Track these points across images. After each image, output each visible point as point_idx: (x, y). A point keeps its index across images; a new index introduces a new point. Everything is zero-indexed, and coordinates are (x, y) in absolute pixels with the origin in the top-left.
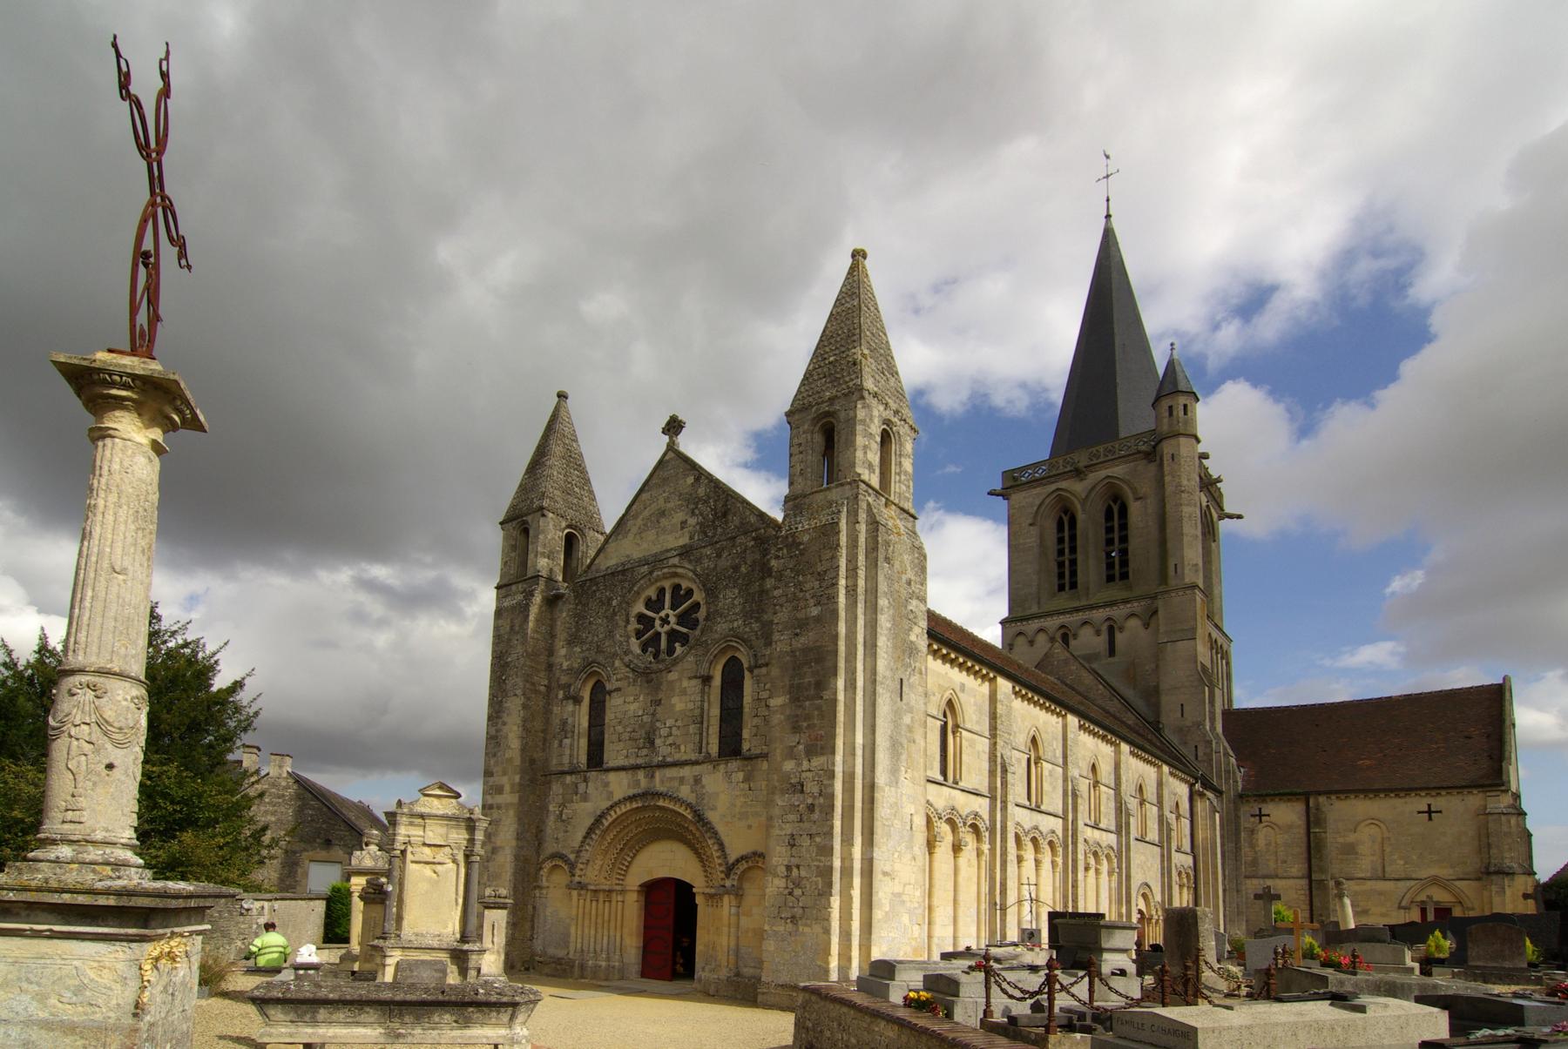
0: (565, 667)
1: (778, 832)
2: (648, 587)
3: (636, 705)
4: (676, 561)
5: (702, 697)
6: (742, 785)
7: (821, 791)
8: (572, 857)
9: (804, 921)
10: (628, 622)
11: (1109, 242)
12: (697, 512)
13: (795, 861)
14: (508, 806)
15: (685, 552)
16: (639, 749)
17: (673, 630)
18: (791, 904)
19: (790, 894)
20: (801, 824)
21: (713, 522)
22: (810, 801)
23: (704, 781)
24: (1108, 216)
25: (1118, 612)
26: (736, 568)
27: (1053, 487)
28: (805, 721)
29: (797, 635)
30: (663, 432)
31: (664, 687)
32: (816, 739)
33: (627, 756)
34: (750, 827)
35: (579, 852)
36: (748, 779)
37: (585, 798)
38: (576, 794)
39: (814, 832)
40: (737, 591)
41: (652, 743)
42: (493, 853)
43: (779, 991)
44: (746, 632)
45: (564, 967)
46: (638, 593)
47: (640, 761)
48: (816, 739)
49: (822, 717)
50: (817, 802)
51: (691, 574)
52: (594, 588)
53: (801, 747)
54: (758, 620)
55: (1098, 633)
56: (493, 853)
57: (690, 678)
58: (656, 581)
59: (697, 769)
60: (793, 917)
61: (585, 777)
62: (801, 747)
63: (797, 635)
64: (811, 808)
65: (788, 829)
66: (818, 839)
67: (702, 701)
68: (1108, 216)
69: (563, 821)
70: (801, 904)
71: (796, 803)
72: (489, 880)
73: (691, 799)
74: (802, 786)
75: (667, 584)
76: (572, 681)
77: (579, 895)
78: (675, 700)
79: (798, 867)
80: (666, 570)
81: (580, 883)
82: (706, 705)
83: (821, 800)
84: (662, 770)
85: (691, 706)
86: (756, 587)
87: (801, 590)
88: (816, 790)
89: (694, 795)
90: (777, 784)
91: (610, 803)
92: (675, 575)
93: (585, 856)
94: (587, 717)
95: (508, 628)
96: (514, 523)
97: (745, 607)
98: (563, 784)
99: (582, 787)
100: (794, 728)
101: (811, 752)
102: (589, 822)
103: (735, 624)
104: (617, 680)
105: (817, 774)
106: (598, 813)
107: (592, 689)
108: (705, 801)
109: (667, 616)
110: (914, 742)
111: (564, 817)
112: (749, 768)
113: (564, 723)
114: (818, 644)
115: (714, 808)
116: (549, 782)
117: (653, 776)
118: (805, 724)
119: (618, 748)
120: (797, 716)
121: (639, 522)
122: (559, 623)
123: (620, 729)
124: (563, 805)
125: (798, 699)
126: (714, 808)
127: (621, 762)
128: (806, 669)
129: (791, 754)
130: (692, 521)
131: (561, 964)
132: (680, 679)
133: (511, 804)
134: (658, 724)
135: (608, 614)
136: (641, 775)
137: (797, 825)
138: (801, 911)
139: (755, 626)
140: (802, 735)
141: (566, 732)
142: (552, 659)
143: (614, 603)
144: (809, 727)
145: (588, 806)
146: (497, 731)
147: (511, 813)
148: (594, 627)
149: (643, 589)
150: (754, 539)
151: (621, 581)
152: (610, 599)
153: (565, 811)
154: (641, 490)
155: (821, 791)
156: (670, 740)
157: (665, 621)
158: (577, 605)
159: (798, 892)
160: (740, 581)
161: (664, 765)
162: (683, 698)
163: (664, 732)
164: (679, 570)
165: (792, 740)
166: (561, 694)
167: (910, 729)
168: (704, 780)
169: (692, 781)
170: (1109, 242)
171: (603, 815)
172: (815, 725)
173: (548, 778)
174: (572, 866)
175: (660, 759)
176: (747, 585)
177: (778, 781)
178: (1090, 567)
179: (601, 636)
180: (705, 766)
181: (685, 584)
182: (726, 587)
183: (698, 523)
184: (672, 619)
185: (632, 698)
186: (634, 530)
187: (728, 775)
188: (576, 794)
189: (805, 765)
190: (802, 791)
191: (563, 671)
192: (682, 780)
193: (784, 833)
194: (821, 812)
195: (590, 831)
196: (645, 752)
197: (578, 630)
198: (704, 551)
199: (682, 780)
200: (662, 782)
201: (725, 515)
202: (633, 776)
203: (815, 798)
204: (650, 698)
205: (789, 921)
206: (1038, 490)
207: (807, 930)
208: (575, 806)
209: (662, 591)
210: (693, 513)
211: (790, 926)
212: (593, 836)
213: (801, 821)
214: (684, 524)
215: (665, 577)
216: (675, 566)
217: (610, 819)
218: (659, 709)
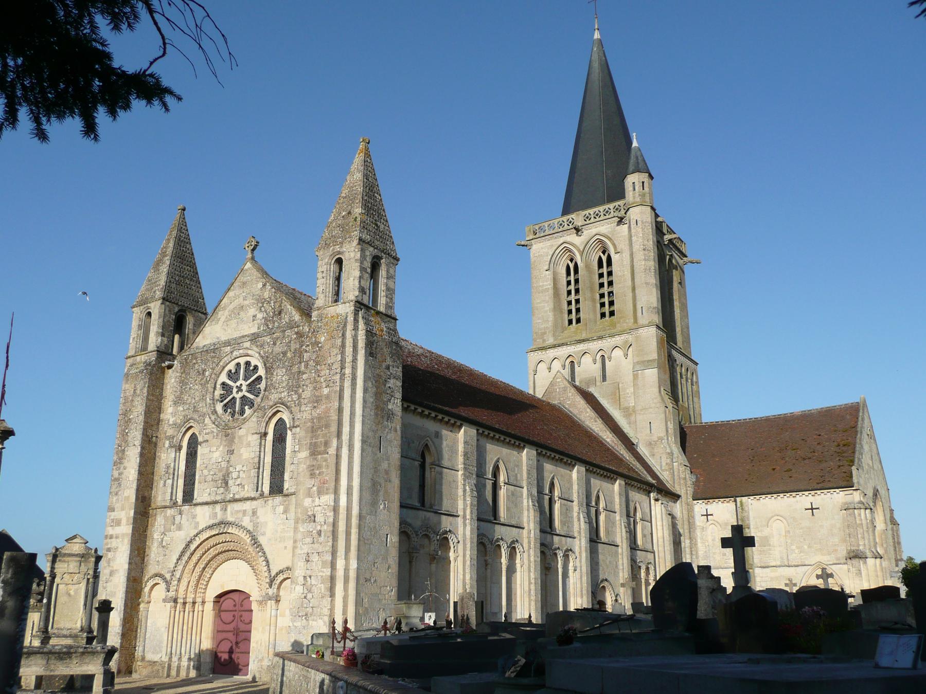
0: (171, 422)
4: (247, 344)
5: (260, 448)
7: (325, 520)
10: (215, 388)
12: (263, 309)
13: (309, 573)
15: (254, 338)
16: (218, 488)
18: (305, 606)
21: (273, 317)
22: (319, 528)
25: (607, 343)
26: (284, 354)
27: (561, 240)
29: (315, 407)
31: (236, 441)
37: (179, 528)
39: (320, 550)
41: (227, 483)
52: (194, 361)
53: (315, 488)
55: (595, 362)
62: (315, 488)
63: (315, 407)
67: (260, 452)
71: (311, 530)
74: (315, 517)
75: (242, 361)
78: (243, 450)
79: (310, 577)
82: (262, 454)
83: (325, 527)
86: (295, 369)
87: (319, 376)
88: (322, 520)
97: (288, 383)
100: (311, 475)
103: (283, 395)
108: (259, 529)
109: (241, 385)
110: (390, 481)
111: (164, 544)
115: (264, 534)
121: (226, 313)
122: (169, 387)
126: (264, 534)
130: (260, 316)
135: (202, 382)
137: (311, 545)
143: (207, 373)
152: (204, 371)
155: (325, 520)
157: (239, 389)
159: (309, 596)
164: (250, 352)
166: (167, 443)
167: (387, 472)
176: (291, 366)
178: (589, 310)
179: (197, 399)
184: (244, 388)
186: (223, 319)
191: (170, 425)
197: (182, 393)
201: (280, 313)
203: (321, 525)
204: (227, 449)
206: (548, 243)
209: (238, 365)
216: (247, 348)
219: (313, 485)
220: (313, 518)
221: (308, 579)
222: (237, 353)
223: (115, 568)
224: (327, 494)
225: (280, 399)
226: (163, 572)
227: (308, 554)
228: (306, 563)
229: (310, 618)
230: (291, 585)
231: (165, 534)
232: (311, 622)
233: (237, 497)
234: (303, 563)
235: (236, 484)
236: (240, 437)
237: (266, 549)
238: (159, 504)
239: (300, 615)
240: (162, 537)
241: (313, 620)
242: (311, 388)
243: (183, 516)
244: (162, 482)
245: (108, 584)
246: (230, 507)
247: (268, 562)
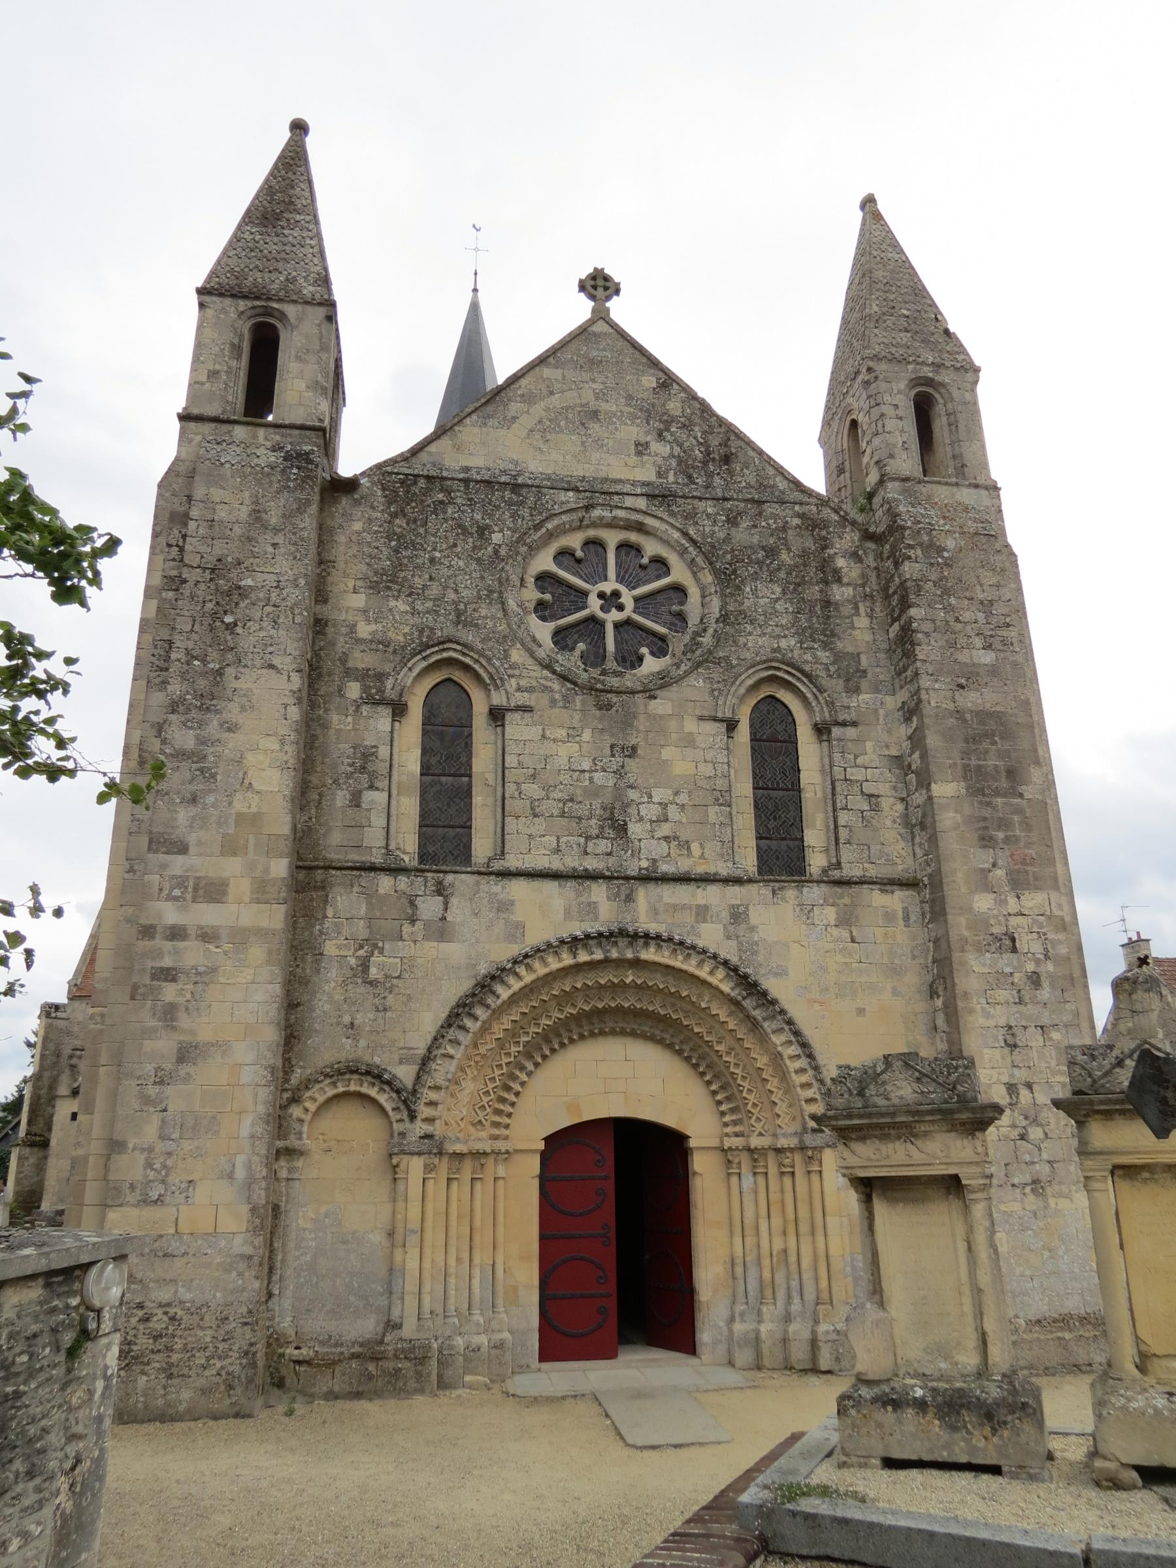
1: (982, 1021)
2: (573, 529)
3: (573, 748)
6: (835, 932)
7: (1046, 949)
8: (405, 1074)
9: (1056, 1187)
11: (474, 311)
13: (1021, 1075)
14: (241, 937)
16: (588, 838)
17: (601, 624)
18: (1027, 1158)
19: (1023, 1137)
20: (1021, 1008)
22: (1030, 967)
23: (755, 917)
24: (475, 290)
28: (999, 828)
30: (582, 287)
32: (1024, 862)
33: (557, 850)
34: (861, 1011)
35: (426, 1061)
36: (846, 920)
37: (441, 930)
38: (413, 922)
39: (1046, 1021)
40: (778, 590)
41: (622, 830)
42: (181, 1060)
43: (1037, 1333)
44: (806, 662)
45: (389, 1365)
46: (551, 535)
47: (591, 864)
48: (1024, 862)
49: (1027, 826)
50: (1041, 970)
51: (677, 535)
53: (1000, 873)
54: (825, 646)
56: (181, 1060)
57: (701, 718)
58: (594, 525)
59: (735, 894)
60: (1035, 1182)
61: (440, 883)
62: (1000, 873)
63: (961, 687)
64: (1035, 980)
65: (1001, 1016)
66: (1056, 1035)
68: (475, 290)
69: (371, 983)
70: (1045, 1156)
71: (1008, 970)
72: (163, 1137)
73: (728, 951)
74: (1013, 940)
75: (612, 538)
76: (388, 667)
77: (429, 1168)
79: (1029, 1086)
80: (621, 513)
81: (428, 1137)
83: (1050, 967)
84: (651, 886)
85: (708, 770)
86: (813, 592)
87: (957, 620)
88: (1037, 948)
89: (734, 943)
90: (966, 933)
91: (515, 950)
92: (640, 528)
93: (441, 1071)
94: (417, 752)
95: (244, 513)
96: (243, 304)
98: (369, 895)
99: (430, 907)
100: (982, 838)
101: (1019, 883)
102: (456, 989)
104: (519, 689)
105: (1035, 921)
106: (483, 969)
107: (759, 702)
108: (761, 958)
111: (373, 972)
112: (847, 900)
113: (367, 756)
114: (998, 709)
115: (781, 973)
116: (323, 886)
117: (629, 898)
118: (1001, 835)
119: (532, 830)
120: (985, 819)
122: (342, 539)
123: (533, 790)
124: (372, 944)
125: (981, 791)
126: (781, 973)
127: (541, 860)
128: (985, 745)
129: (983, 882)
131: (376, 1359)
132: (679, 716)
133: (262, 934)
134: (632, 795)
136: (599, 892)
137: (1015, 1008)
138: (1047, 1168)
139: (824, 656)
140: (1000, 853)
141: (373, 776)
142: (324, 611)
143: (497, 538)
144: (1007, 840)
145: (453, 951)
146: (202, 741)
147: (257, 952)
148: (445, 571)
149: (562, 531)
150: (798, 515)
151: (510, 503)
153: (376, 959)
154: (541, 361)
155: (1046, 949)
156: (665, 829)
157: (611, 600)
158: (394, 515)
159: (1035, 1133)
160: (782, 575)
161: (649, 878)
162: (689, 752)
163: (650, 811)
164: (649, 521)
165: (983, 858)
166: (354, 690)
168: (751, 914)
169: (725, 915)
170: (474, 311)
171: (497, 976)
172: (1017, 839)
173: (319, 875)
174: (408, 1101)
175: (644, 864)
176: (799, 585)
177: (969, 928)
180: (753, 889)
181: (651, 548)
182: (755, 577)
183: (672, 456)
185: (564, 732)
186: (527, 422)
187: (808, 911)
188: (413, 922)
189: (1012, 905)
190: (1014, 950)
192: (702, 913)
193: (992, 1023)
194: (1053, 986)
195: (455, 1017)
196: (603, 845)
198: (701, 505)
199: (702, 913)
200: (654, 912)
201: (727, 459)
202: (579, 894)
203: (1038, 962)
204: (608, 740)
205: (1028, 1190)
207: (1063, 1204)
208: (405, 949)
210: (660, 436)
211: (1031, 1201)
212: (468, 1023)
213: (1021, 1001)
214: (641, 448)
215: (612, 525)
217: (516, 985)
218: (631, 764)
219: (994, 865)
220: (1008, 942)
221: (1024, 1092)
222: (607, 514)
223: (205, 1034)
224: (1037, 889)
225: (775, 650)
226: (377, 1060)
227: (1010, 1027)
228: (1007, 1050)
229: (1049, 1190)
230: (998, 1110)
231: (375, 946)
232: (1052, 1202)
233: (665, 868)
234: (997, 1052)
235: (659, 834)
236: (654, 718)
237: (796, 1011)
238: (333, 856)
239: (1016, 1181)
240: (361, 953)
241: (1061, 1195)
242: (942, 643)
243: (454, 901)
244: (341, 797)
245: (169, 1090)
246: (644, 895)
247: (804, 1045)
